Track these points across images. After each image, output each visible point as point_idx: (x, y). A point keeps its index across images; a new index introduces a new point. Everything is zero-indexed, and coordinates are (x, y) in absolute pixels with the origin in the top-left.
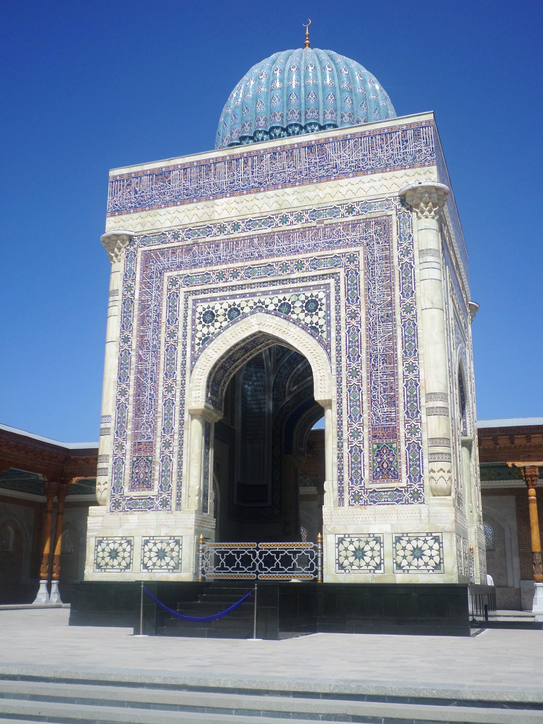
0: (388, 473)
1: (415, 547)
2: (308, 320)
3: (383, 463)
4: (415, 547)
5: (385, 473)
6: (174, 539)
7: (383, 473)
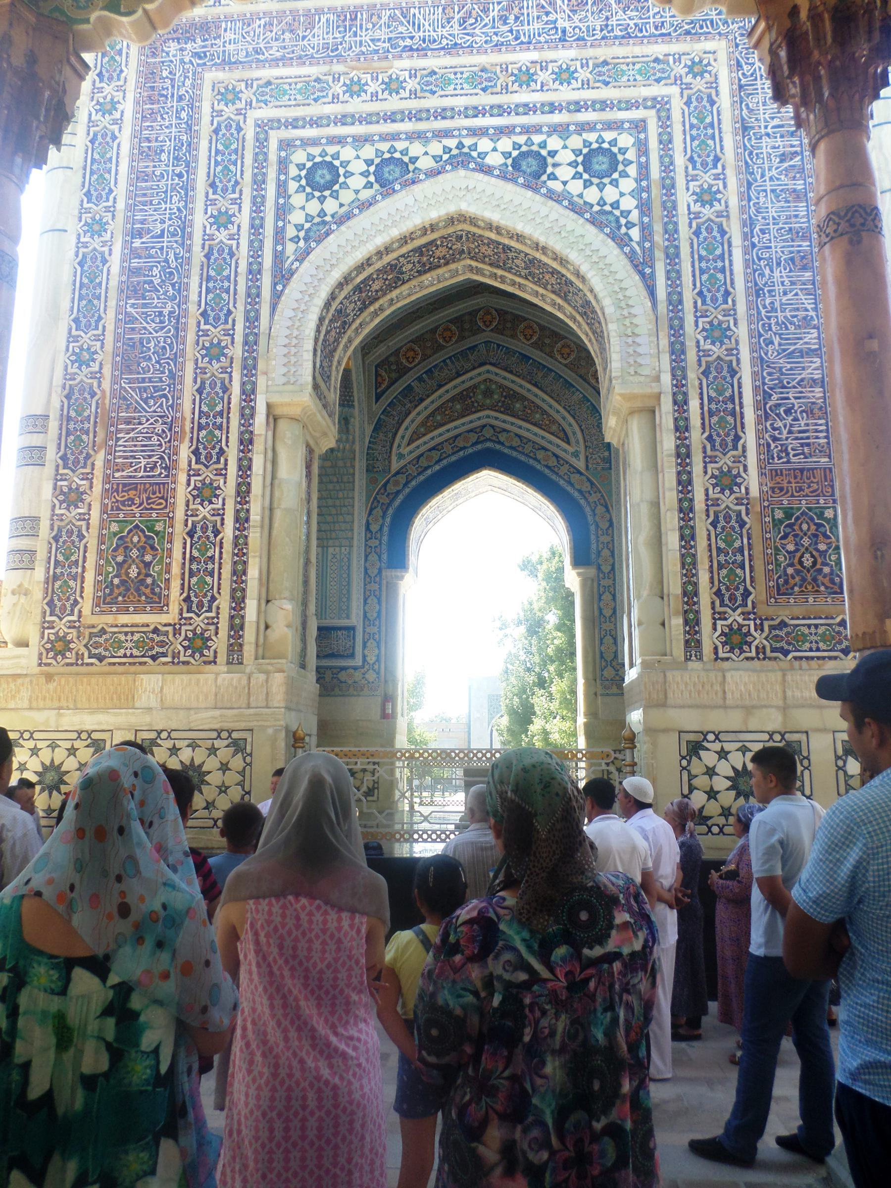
0: (815, 580)
1: (56, 763)
2: (592, 195)
3: (802, 556)
4: (56, 763)
5: (809, 578)
6: (230, 736)
7: (804, 580)
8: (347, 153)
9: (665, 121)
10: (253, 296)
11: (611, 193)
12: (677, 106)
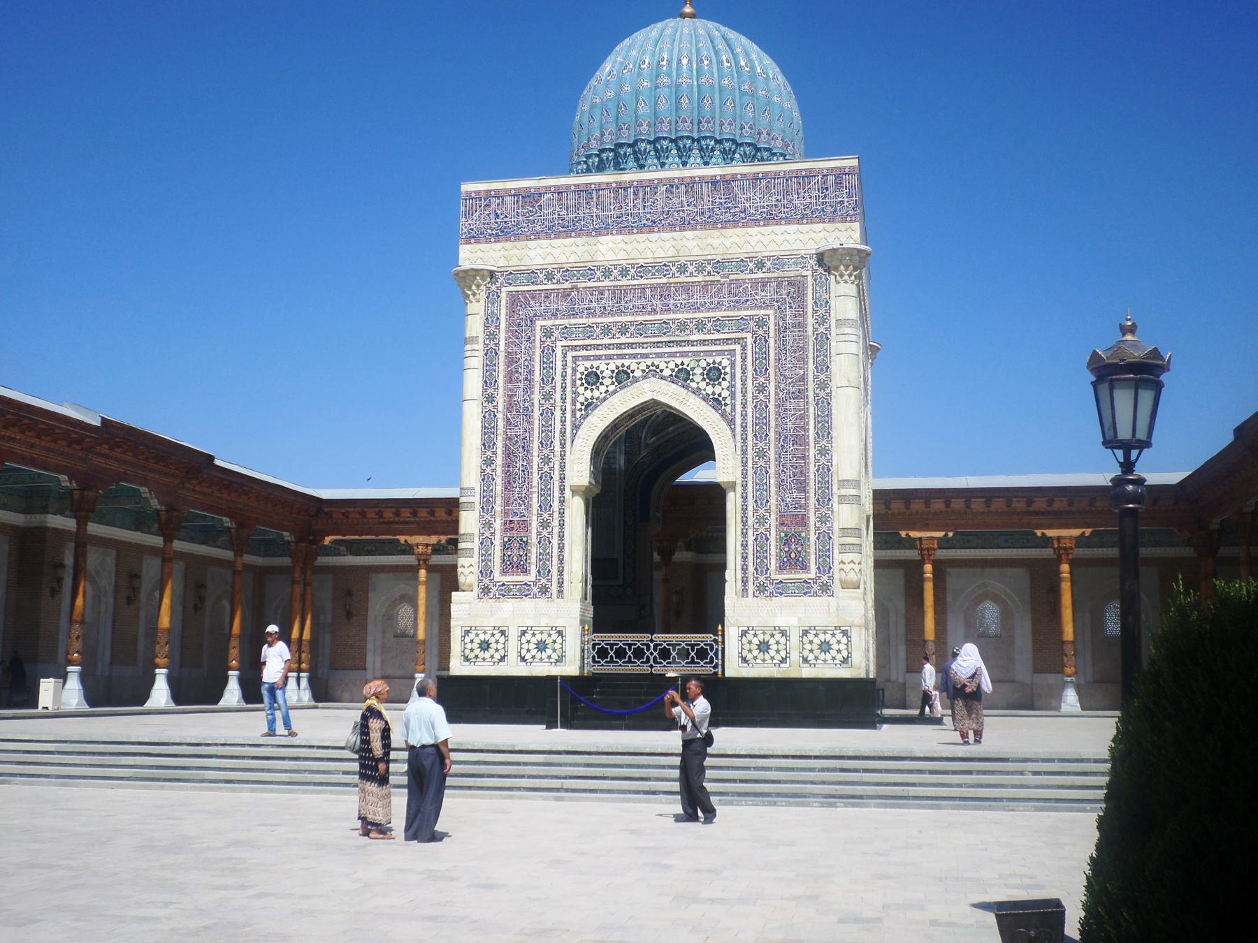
2: (710, 390)
8: (725, 384)
9: (744, 348)
10: (563, 433)
11: (718, 390)
12: (750, 341)
